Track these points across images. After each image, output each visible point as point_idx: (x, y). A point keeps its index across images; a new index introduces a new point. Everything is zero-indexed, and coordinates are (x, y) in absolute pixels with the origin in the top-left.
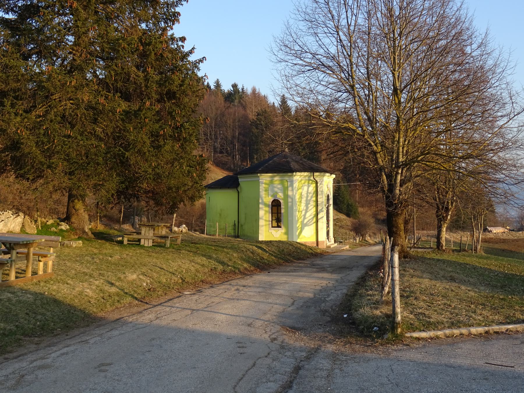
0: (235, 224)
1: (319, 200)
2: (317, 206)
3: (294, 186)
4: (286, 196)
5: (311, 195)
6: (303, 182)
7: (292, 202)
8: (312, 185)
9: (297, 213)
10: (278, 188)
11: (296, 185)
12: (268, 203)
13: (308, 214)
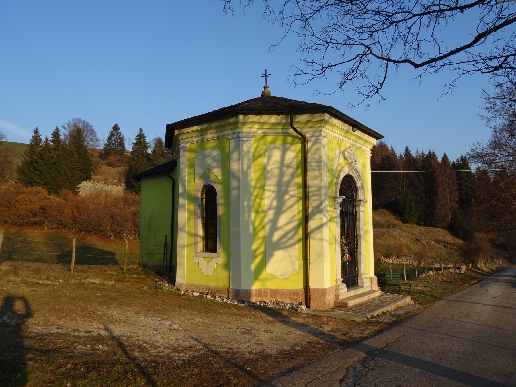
0: (166, 243)
1: (310, 182)
2: (305, 197)
3: (245, 148)
4: (228, 173)
5: (291, 170)
6: (269, 139)
7: (238, 188)
8: (293, 147)
9: (253, 215)
10: (213, 158)
11: (249, 146)
12: (193, 193)
13: (283, 220)
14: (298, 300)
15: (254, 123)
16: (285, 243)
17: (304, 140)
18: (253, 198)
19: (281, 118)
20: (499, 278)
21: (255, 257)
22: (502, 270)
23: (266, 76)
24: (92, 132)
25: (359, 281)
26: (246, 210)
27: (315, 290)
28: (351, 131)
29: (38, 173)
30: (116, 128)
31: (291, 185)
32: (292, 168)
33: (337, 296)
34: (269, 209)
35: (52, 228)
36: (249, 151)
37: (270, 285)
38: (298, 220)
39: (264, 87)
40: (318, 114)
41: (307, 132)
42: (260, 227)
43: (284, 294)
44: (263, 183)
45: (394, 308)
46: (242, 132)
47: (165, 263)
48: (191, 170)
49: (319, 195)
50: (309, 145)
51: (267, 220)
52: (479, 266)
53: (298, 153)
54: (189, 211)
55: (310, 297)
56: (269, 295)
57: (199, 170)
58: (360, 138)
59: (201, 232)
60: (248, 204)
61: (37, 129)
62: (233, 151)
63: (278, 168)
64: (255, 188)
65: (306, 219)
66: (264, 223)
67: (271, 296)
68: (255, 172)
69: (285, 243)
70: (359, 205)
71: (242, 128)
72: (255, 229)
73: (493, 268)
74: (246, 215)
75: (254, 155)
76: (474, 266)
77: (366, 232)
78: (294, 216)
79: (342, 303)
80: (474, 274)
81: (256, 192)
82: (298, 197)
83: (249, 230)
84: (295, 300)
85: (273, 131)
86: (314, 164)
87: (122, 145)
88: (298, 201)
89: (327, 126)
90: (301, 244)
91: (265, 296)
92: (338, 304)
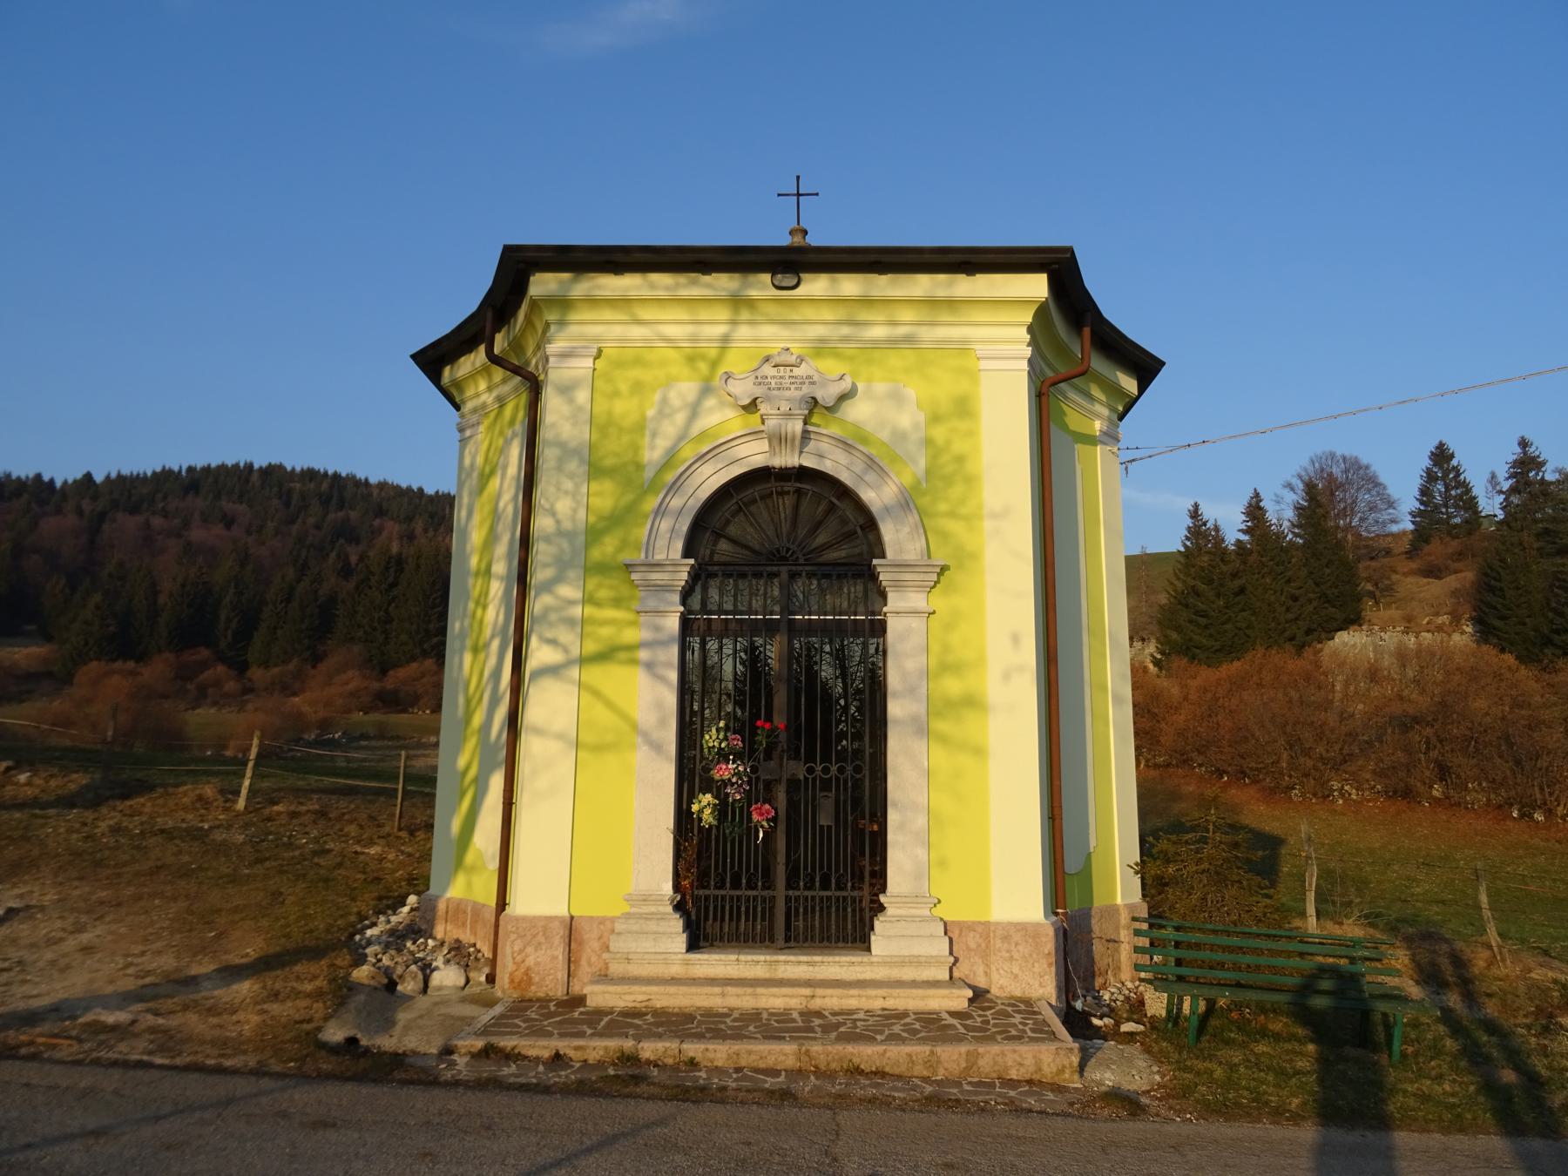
18: (471, 605)
21: (463, 794)
24: (1373, 482)
29: (1203, 621)
30: (1441, 455)
35: (1156, 766)
36: (472, 465)
58: (866, 302)
61: (1196, 506)
72: (468, 702)
74: (456, 660)
87: (1470, 504)
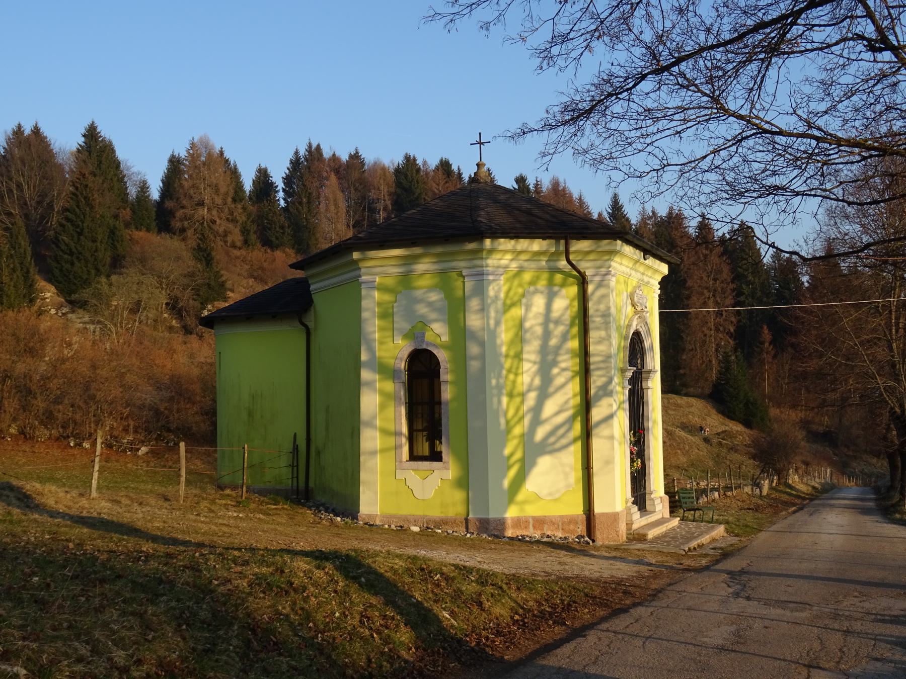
0: (296, 449)
1: (592, 348)
2: (585, 372)
3: (491, 292)
4: (460, 334)
5: (561, 329)
6: (527, 276)
7: (482, 357)
8: (564, 291)
9: (505, 400)
10: (430, 304)
11: (497, 288)
13: (550, 408)
14: (576, 532)
15: (506, 252)
16: (554, 443)
17: (582, 281)
18: (504, 372)
19: (548, 245)
20: (833, 502)
21: (509, 468)
22: (832, 489)
23: (480, 143)
25: (648, 503)
26: (495, 392)
27: (603, 514)
28: (642, 260)
31: (562, 351)
32: (563, 324)
33: (629, 525)
34: (529, 390)
36: (497, 297)
37: (532, 511)
38: (574, 407)
39: (478, 165)
40: (606, 242)
41: (588, 267)
42: (516, 419)
43: (554, 524)
44: (519, 349)
45: (709, 540)
46: (487, 266)
47: (295, 484)
48: (384, 323)
49: (606, 368)
50: (590, 288)
51: (525, 408)
52: (790, 482)
53: (572, 300)
54: (382, 393)
55: (595, 526)
56: (531, 526)
57: (402, 324)
59: (405, 430)
60: (498, 383)
62: (470, 297)
63: (541, 324)
64: (507, 356)
65: (586, 405)
66: (521, 413)
67: (534, 527)
68: (507, 330)
69: (554, 443)
70: (647, 378)
71: (487, 258)
72: (508, 422)
73: (817, 485)
74: (495, 400)
75: (504, 304)
76: (783, 481)
77: (655, 422)
78: (567, 402)
79: (638, 534)
80: (785, 497)
81: (508, 364)
82: (573, 371)
83: (499, 424)
84: (572, 532)
85: (533, 265)
86: (598, 319)
88: (573, 377)
89: (617, 259)
90: (579, 444)
91: (526, 528)
92: (631, 537)
